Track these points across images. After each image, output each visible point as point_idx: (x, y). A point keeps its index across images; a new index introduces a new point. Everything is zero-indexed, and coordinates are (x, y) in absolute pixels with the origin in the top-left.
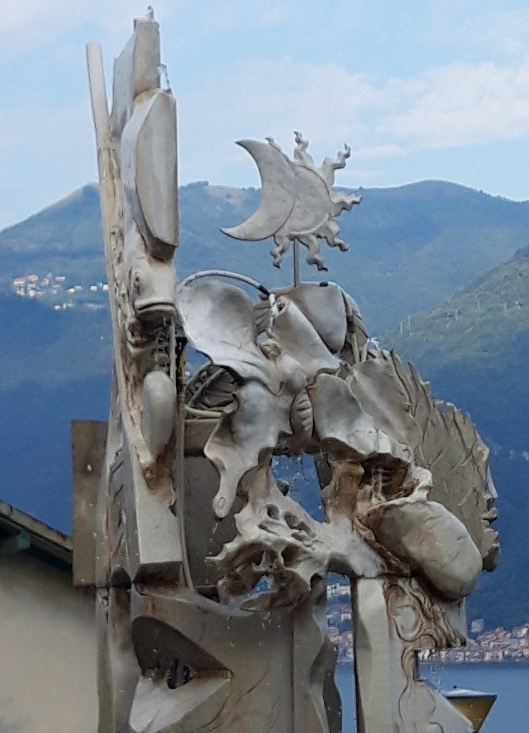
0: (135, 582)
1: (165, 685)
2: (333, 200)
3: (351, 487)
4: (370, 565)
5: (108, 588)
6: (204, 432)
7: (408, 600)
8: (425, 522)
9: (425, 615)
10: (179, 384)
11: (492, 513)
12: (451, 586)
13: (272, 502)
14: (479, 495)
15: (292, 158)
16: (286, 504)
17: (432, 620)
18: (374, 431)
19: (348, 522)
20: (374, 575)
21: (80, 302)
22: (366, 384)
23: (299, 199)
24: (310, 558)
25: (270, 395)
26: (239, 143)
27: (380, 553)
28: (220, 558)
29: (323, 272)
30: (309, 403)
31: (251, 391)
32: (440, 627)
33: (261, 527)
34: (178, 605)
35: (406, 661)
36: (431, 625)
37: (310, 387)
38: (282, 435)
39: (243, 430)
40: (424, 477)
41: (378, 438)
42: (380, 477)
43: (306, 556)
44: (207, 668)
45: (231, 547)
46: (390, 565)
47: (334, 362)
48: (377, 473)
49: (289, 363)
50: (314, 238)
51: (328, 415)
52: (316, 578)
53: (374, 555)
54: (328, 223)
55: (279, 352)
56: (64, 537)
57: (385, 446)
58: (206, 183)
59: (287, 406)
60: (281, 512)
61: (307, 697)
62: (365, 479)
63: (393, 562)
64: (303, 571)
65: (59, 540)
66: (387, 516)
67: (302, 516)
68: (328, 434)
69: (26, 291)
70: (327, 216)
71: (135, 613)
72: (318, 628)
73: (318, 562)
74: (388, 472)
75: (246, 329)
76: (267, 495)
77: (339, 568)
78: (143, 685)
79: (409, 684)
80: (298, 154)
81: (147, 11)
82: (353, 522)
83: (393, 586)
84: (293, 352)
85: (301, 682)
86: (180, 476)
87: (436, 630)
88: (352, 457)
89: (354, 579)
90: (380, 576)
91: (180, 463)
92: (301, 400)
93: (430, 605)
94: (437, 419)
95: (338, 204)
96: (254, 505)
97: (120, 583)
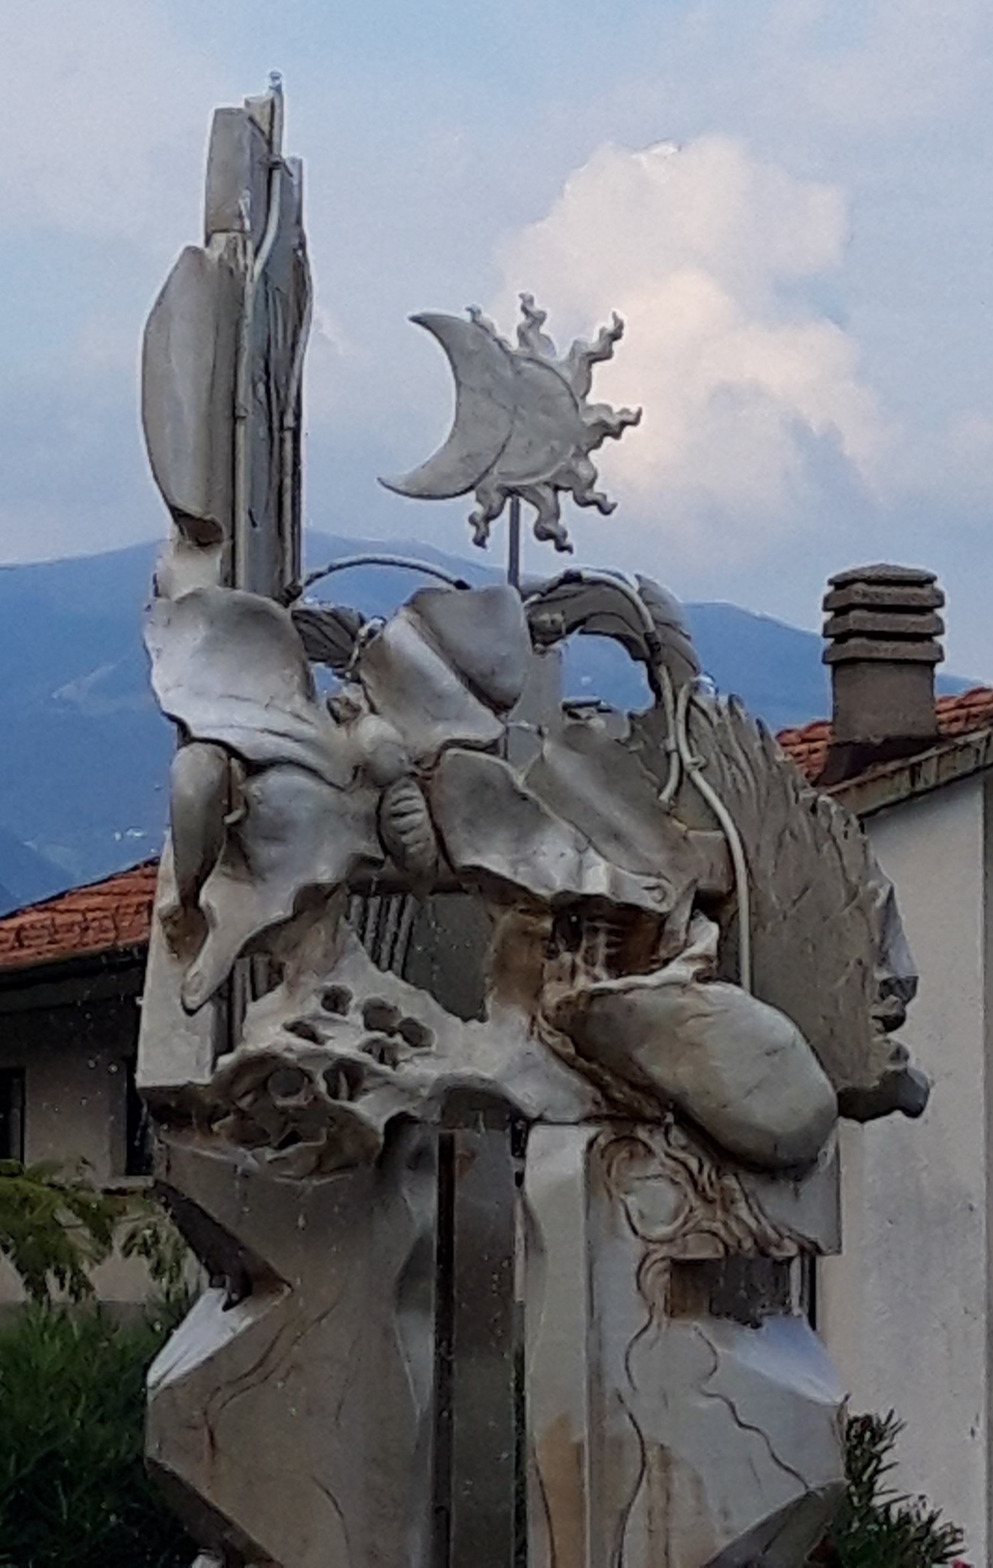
2: (585, 420)
4: (561, 1096)
8: (687, 1021)
12: (748, 1142)
13: (344, 982)
14: (865, 974)
15: (514, 343)
16: (367, 982)
17: (718, 1204)
18: (570, 853)
19: (525, 1021)
23: (522, 419)
24: (388, 1083)
25: (326, 790)
27: (590, 1077)
29: (565, 554)
30: (420, 804)
32: (739, 1219)
33: (296, 1028)
35: (648, 1279)
36: (715, 1213)
37: (424, 770)
39: (266, 853)
42: (602, 939)
43: (379, 1080)
48: (596, 930)
50: (547, 493)
53: (576, 1081)
54: (574, 463)
57: (597, 881)
63: (618, 1096)
66: (596, 1008)
67: (413, 1004)
68: (468, 859)
70: (572, 450)
72: (408, 1212)
74: (632, 935)
75: (288, 672)
79: (655, 1322)
81: (268, 82)
82: (534, 1019)
87: (725, 1224)
88: (525, 901)
92: (395, 797)
93: (713, 1177)
94: (800, 826)
95: (594, 425)
96: (292, 987)
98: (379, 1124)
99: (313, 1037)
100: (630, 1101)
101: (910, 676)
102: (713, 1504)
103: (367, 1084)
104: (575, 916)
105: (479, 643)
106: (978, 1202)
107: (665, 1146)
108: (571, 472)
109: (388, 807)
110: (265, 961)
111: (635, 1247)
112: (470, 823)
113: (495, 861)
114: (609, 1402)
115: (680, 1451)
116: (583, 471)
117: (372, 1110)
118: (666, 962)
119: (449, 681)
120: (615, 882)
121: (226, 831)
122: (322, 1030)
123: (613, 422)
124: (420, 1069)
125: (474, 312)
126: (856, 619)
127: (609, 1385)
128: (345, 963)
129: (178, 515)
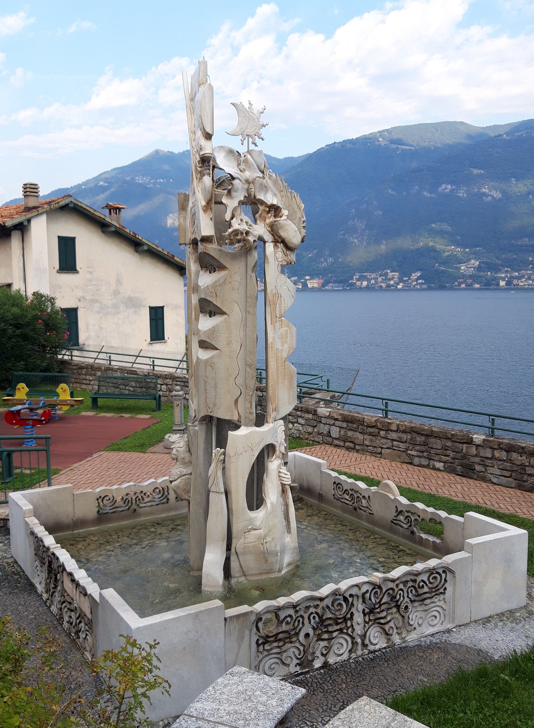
0: (200, 241)
1: (208, 272)
3: (264, 214)
4: (270, 238)
5: (190, 244)
6: (222, 196)
7: (280, 250)
10: (213, 180)
11: (304, 225)
12: (292, 246)
15: (247, 109)
20: (270, 241)
22: (269, 182)
27: (272, 235)
28: (227, 233)
31: (236, 182)
34: (212, 249)
38: (245, 197)
39: (234, 194)
40: (285, 212)
41: (273, 199)
44: (222, 267)
45: (230, 230)
46: (275, 239)
47: (261, 175)
50: (254, 136)
51: (259, 191)
52: (254, 241)
53: (271, 236)
55: (245, 170)
57: (275, 202)
59: (247, 187)
60: (244, 221)
61: (251, 276)
62: (269, 212)
64: (251, 239)
65: (156, 247)
67: (250, 222)
71: (199, 251)
73: (255, 236)
74: (275, 210)
76: (240, 215)
77: (261, 239)
78: (202, 273)
80: (249, 108)
83: (276, 245)
84: (249, 171)
85: (249, 272)
86: (213, 209)
89: (265, 242)
90: (272, 242)
91: (213, 205)
96: (237, 218)
97: (195, 243)
101: (36, 198)
106: (48, 269)
115: (282, 295)
126: (28, 190)
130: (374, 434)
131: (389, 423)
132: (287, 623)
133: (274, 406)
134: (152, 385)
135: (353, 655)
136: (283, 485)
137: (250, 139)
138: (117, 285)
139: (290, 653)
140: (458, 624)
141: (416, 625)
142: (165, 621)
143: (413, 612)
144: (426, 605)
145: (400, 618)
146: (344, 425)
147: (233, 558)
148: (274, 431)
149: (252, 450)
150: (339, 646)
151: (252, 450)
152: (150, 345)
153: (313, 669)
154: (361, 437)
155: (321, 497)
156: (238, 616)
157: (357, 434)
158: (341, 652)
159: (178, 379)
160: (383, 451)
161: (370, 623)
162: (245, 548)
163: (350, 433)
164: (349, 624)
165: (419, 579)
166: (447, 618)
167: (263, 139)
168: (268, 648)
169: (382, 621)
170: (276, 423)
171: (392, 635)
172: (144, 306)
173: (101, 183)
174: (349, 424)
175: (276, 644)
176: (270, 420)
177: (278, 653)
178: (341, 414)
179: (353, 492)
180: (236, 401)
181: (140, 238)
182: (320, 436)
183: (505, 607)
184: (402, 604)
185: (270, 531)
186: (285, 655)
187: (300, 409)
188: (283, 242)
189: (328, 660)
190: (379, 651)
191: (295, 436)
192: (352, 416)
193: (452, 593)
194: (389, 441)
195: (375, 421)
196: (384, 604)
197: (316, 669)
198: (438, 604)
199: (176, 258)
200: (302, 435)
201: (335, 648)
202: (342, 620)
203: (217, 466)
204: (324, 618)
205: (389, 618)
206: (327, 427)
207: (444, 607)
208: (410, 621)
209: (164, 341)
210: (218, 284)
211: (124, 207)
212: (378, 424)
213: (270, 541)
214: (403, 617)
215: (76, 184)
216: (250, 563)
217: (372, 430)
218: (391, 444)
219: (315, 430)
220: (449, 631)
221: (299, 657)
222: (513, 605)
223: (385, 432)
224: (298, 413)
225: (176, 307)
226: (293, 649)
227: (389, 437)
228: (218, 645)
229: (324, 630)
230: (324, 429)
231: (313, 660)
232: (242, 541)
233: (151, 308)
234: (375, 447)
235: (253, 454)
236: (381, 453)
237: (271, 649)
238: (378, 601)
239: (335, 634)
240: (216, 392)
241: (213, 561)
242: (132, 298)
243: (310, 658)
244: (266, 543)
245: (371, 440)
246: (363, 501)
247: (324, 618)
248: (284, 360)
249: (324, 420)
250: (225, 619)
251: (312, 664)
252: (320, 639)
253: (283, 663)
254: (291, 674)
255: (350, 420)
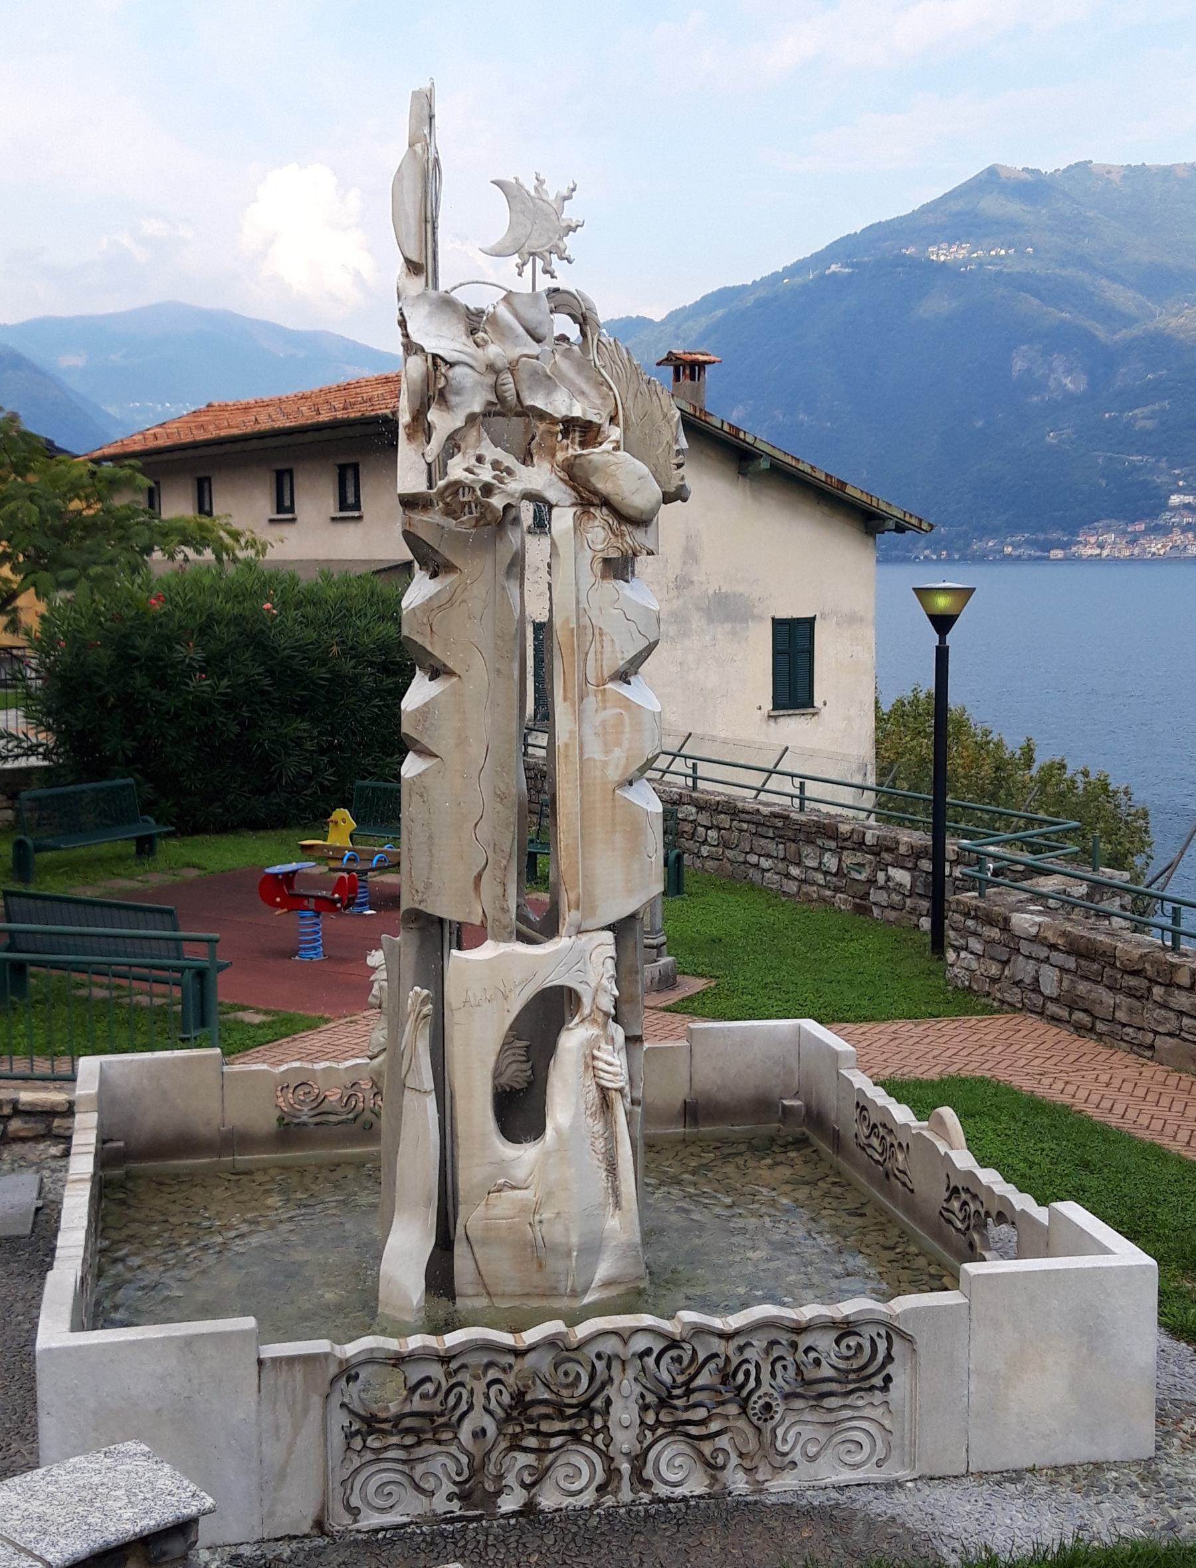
9: (613, 533)
12: (631, 512)
15: (533, 193)
16: (492, 452)
18: (568, 400)
20: (568, 503)
21: (980, 265)
25: (476, 374)
26: (493, 182)
27: (574, 488)
30: (511, 380)
37: (512, 367)
39: (453, 399)
42: (577, 434)
44: (449, 568)
46: (582, 498)
49: (494, 351)
50: (547, 254)
53: (569, 490)
56: (797, 460)
57: (577, 412)
58: (1091, 162)
65: (794, 463)
66: (578, 461)
67: (509, 460)
68: (528, 402)
69: (938, 256)
74: (587, 432)
98: (501, 507)
99: (472, 473)
100: (590, 499)
102: (618, 649)
103: (496, 491)
104: (570, 425)
105: (531, 315)
107: (601, 514)
108: (557, 247)
109: (500, 381)
110: (453, 445)
111: (589, 553)
112: (530, 388)
113: (540, 404)
114: (581, 612)
115: (605, 630)
116: (562, 246)
117: (498, 502)
118: (601, 444)
119: (521, 331)
120: (584, 412)
121: (435, 390)
122: (476, 470)
123: (573, 225)
124: (514, 486)
125: (516, 179)
127: (581, 606)
128: (483, 444)
129: (408, 261)
130: (1139, 994)
131: (1173, 965)
132: (424, 1396)
133: (573, 897)
134: (688, 827)
135: (609, 1501)
136: (603, 1091)
137: (540, 263)
138: (684, 563)
139: (436, 1465)
140: (928, 1473)
141: (796, 1455)
142: (112, 1344)
143: (787, 1423)
144: (830, 1410)
145: (750, 1432)
146: (1071, 963)
147: (460, 1249)
148: (583, 959)
149: (506, 998)
150: (570, 1471)
151: (506, 998)
152: (772, 723)
153: (494, 1514)
154: (1108, 998)
155: (836, 1140)
156: (291, 1360)
157: (1101, 989)
158: (576, 1487)
159: (743, 816)
160: (1158, 1043)
161: (660, 1431)
162: (487, 1228)
163: (1083, 987)
164: (598, 1422)
165: (805, 1341)
166: (895, 1453)
167: (570, 262)
168: (376, 1445)
169: (693, 1430)
170: (584, 938)
171: (723, 1467)
172: (759, 618)
173: (834, 268)
174: (1083, 962)
175: (394, 1440)
176: (563, 930)
177: (404, 1462)
178: (1064, 934)
179: (883, 1128)
180: (479, 877)
181: (750, 439)
182: (1016, 990)
183: (1080, 1450)
184: (754, 1398)
185: (550, 1194)
186: (420, 1469)
187: (973, 913)
188: (606, 503)
189: (540, 1499)
190: (681, 1501)
191: (960, 985)
192: (1089, 939)
193: (907, 1393)
194: (1171, 1015)
195: (1141, 956)
196: (702, 1389)
197: (502, 1516)
198: (867, 1412)
199: (849, 490)
200: (977, 981)
201: (559, 1473)
202: (576, 1410)
203: (416, 1028)
204: (528, 1398)
205: (714, 1426)
206: (1031, 966)
207: (887, 1423)
208: (779, 1443)
209: (811, 710)
210: (435, 604)
211: (712, 358)
212: (1147, 966)
213: (549, 1220)
214: (758, 1429)
215: (767, 273)
216: (501, 1265)
217: (1133, 981)
218: (1176, 1023)
219: (1006, 972)
220: (891, 1486)
221: (458, 1479)
222: (1111, 1451)
223: (1163, 989)
224: (970, 923)
225: (853, 619)
226: (442, 1459)
227: (1172, 1005)
228: (242, 1416)
229: (528, 1426)
230: (1023, 969)
231: (498, 1493)
232: (480, 1211)
233: (777, 623)
234: (1139, 1029)
235: (507, 1007)
236: (1151, 1047)
237: (386, 1449)
238: (680, 1379)
239: (556, 1442)
240: (432, 856)
241: (406, 1250)
242: (727, 596)
243: (490, 1486)
244: (540, 1222)
245: (1130, 1010)
246: (900, 1157)
247: (528, 1398)
248: (611, 787)
249: (1025, 947)
250: (260, 1362)
251: (495, 1503)
252: (516, 1446)
253: (418, 1488)
254: (436, 1515)
255: (1084, 951)
